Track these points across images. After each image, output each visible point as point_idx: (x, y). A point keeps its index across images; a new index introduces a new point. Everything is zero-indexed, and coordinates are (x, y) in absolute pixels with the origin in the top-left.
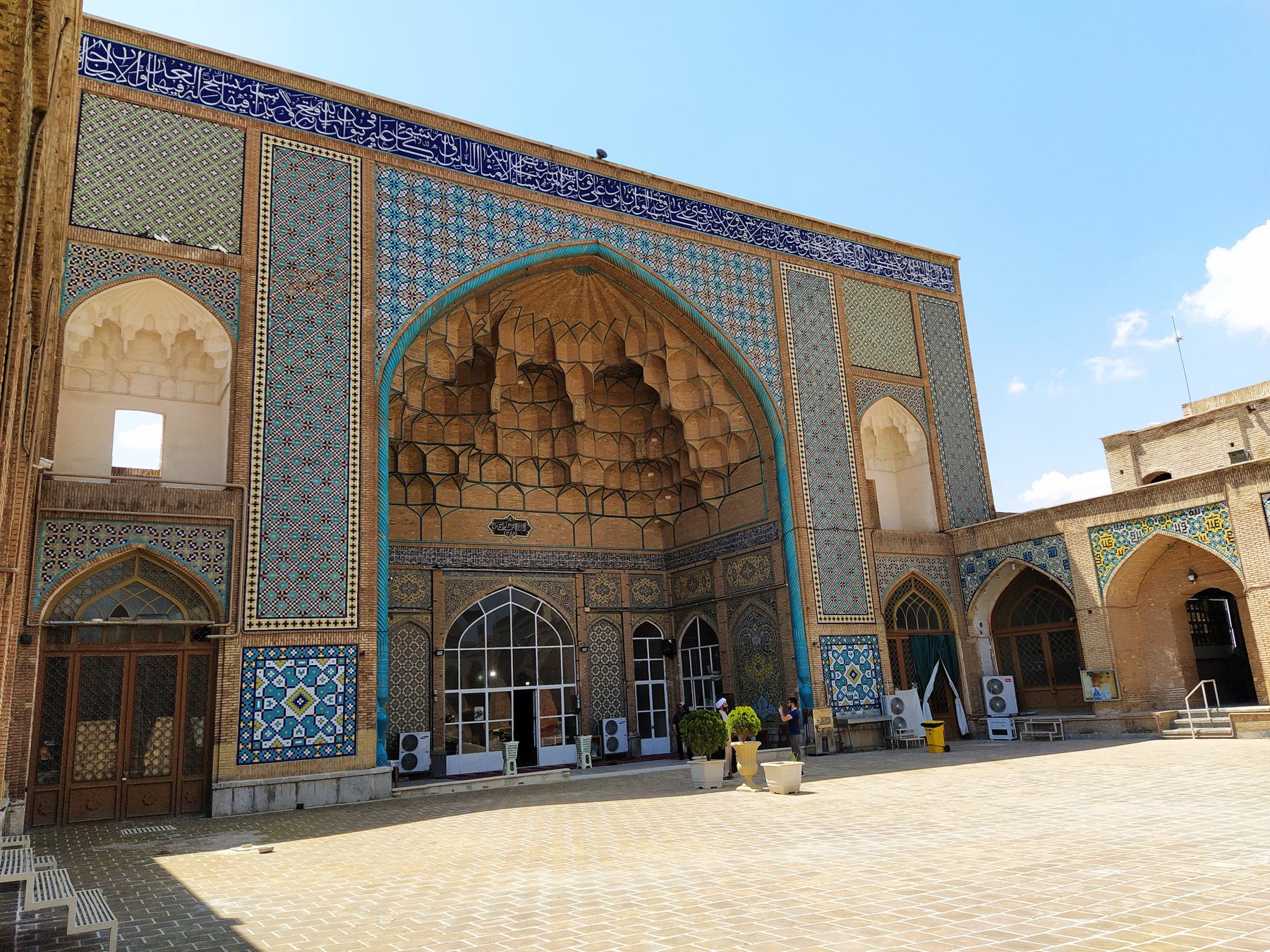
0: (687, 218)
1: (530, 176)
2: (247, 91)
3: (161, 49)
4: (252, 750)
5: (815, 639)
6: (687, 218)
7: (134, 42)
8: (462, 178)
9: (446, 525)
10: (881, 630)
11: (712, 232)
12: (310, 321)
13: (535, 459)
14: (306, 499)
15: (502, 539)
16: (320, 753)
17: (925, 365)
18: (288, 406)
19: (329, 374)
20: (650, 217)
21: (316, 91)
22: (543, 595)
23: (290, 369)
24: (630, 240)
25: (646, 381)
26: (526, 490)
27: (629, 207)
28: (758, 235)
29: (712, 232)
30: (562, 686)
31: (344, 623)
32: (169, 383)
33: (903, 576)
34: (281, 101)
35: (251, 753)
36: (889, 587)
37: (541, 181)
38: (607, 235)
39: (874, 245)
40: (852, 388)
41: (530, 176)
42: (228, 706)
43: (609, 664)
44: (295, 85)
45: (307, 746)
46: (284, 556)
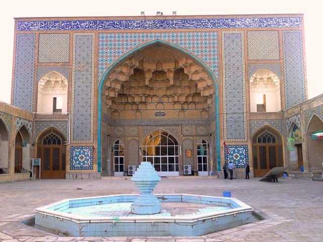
7: (48, 20)
8: (119, 31)
9: (142, 114)
12: (83, 75)
15: (158, 117)
16: (86, 168)
17: (281, 56)
18: (79, 95)
19: (87, 86)
21: (85, 19)
24: (166, 37)
26: (164, 104)
28: (214, 25)
30: (175, 156)
32: (62, 91)
33: (262, 126)
34: (77, 24)
35: (73, 167)
36: (254, 131)
39: (262, 17)
40: (248, 66)
44: (80, 19)
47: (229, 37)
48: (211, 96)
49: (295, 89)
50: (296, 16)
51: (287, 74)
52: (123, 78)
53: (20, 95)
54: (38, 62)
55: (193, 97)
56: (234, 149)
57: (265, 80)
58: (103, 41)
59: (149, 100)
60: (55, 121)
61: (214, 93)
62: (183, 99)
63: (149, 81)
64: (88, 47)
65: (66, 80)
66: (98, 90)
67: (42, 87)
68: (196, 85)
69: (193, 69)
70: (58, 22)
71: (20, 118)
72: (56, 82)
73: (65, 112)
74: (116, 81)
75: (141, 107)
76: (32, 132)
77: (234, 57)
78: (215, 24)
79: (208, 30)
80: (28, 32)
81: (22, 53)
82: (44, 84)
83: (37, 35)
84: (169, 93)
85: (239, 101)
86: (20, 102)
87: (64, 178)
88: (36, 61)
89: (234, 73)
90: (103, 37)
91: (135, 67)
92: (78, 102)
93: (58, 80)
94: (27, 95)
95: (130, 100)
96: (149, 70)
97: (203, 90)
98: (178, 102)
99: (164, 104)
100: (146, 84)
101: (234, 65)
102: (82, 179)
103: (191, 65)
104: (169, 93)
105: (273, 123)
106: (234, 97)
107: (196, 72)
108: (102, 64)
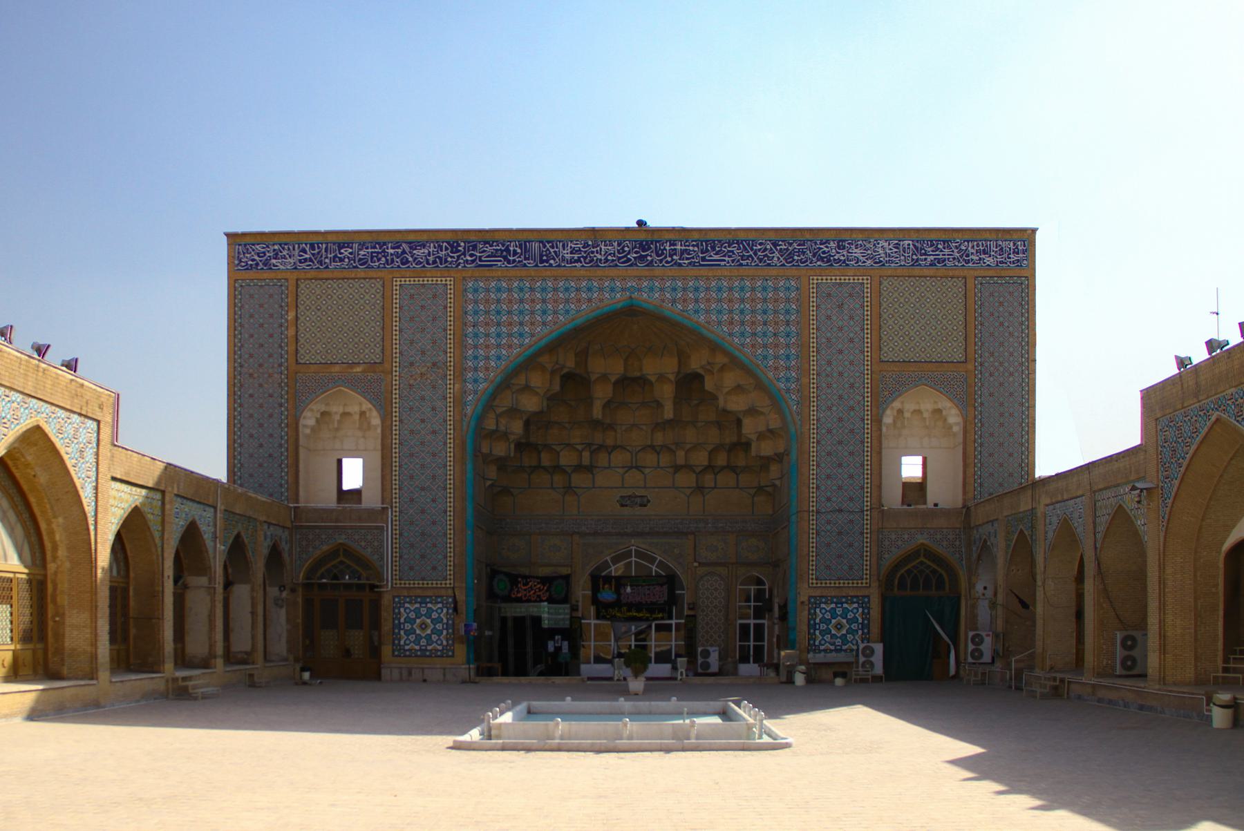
0: (716, 257)
1: (576, 256)
2: (384, 251)
3: (334, 239)
5: (805, 599)
6: (716, 257)
7: (320, 239)
8: (523, 272)
11: (741, 265)
13: (652, 447)
14: (423, 511)
17: (971, 349)
19: (434, 432)
20: (680, 265)
21: (425, 238)
23: (412, 432)
24: (655, 290)
25: (707, 388)
27: (661, 261)
28: (789, 257)
29: (741, 265)
34: (404, 252)
36: (890, 558)
37: (585, 258)
38: (640, 290)
41: (576, 256)
42: (386, 627)
43: (715, 607)
44: (411, 238)
46: (412, 546)
47: (829, 295)
48: (779, 458)
49: (1001, 444)
50: (1015, 237)
51: (982, 404)
52: (531, 404)
53: (251, 456)
54: (297, 363)
55: (729, 451)
57: (926, 415)
58: (476, 302)
59: (602, 459)
60: (351, 528)
61: (787, 453)
62: (701, 458)
63: (604, 407)
64: (434, 319)
65: (375, 413)
66: (463, 443)
67: (308, 431)
68: (739, 422)
69: (730, 379)
70: (348, 245)
71: (269, 524)
72: (345, 415)
73: (372, 500)
74: (513, 412)
75: (577, 479)
76: (290, 554)
77: (840, 352)
78: (791, 255)
79: (773, 272)
80: (265, 275)
81: (252, 336)
82: (312, 422)
83: (292, 282)
84: (659, 439)
85: (851, 477)
86: (251, 476)
88: (292, 360)
89: (841, 397)
90: (476, 290)
91: (565, 371)
92: (412, 477)
93: (349, 409)
94: (270, 455)
95: (546, 460)
96: (604, 377)
97: (758, 439)
98: (688, 467)
100: (595, 416)
101: (841, 374)
102: (425, 681)
103: (723, 368)
104: (659, 439)
106: (840, 465)
107: (739, 389)
108: (476, 369)
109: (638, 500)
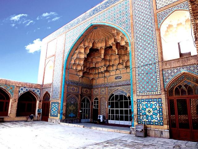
4: (160, 122)
10: (163, 97)
22: (124, 90)
30: (129, 109)
31: (157, 93)
35: (51, 116)
45: (152, 122)
56: (146, 103)
59: (111, 69)
66: (63, 67)
87: (47, 121)
99: (120, 70)
105: (192, 68)
109: (119, 77)
